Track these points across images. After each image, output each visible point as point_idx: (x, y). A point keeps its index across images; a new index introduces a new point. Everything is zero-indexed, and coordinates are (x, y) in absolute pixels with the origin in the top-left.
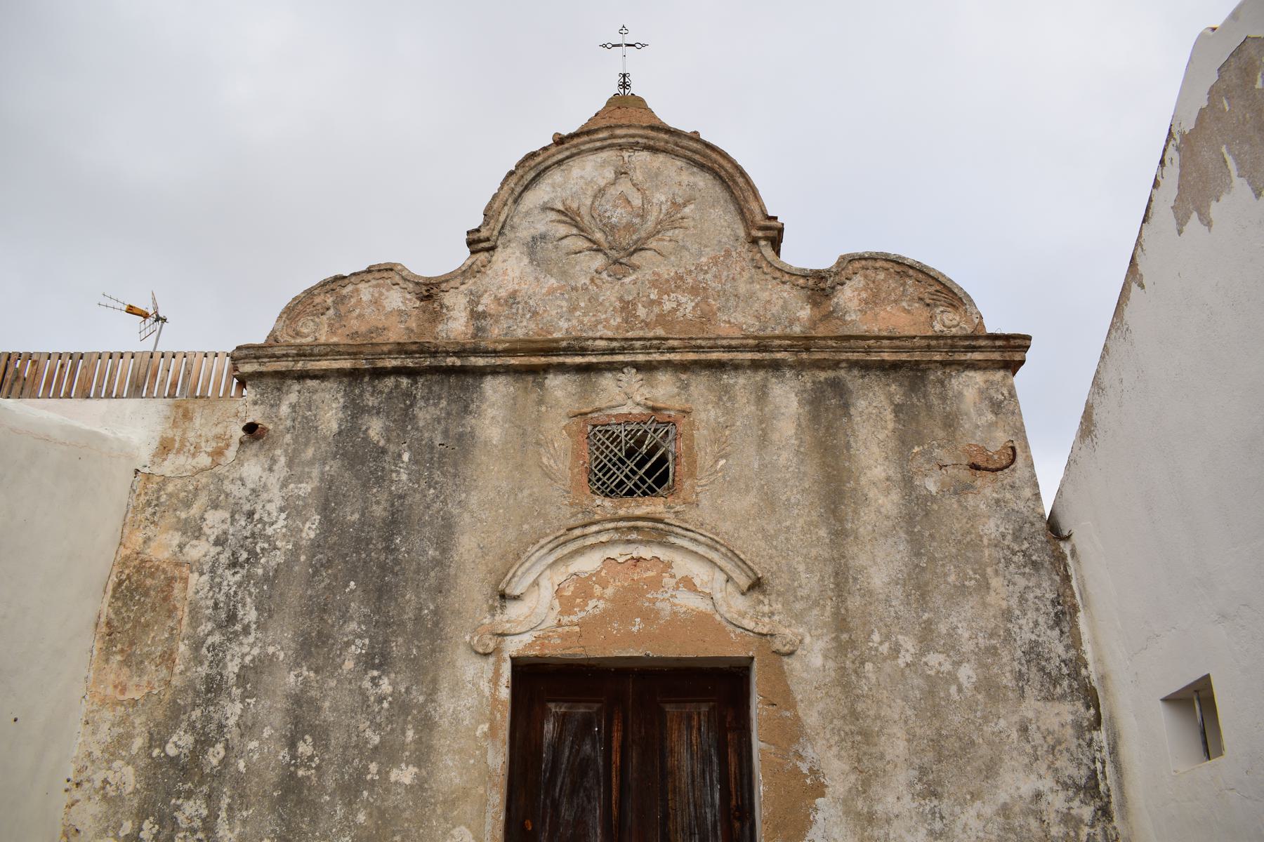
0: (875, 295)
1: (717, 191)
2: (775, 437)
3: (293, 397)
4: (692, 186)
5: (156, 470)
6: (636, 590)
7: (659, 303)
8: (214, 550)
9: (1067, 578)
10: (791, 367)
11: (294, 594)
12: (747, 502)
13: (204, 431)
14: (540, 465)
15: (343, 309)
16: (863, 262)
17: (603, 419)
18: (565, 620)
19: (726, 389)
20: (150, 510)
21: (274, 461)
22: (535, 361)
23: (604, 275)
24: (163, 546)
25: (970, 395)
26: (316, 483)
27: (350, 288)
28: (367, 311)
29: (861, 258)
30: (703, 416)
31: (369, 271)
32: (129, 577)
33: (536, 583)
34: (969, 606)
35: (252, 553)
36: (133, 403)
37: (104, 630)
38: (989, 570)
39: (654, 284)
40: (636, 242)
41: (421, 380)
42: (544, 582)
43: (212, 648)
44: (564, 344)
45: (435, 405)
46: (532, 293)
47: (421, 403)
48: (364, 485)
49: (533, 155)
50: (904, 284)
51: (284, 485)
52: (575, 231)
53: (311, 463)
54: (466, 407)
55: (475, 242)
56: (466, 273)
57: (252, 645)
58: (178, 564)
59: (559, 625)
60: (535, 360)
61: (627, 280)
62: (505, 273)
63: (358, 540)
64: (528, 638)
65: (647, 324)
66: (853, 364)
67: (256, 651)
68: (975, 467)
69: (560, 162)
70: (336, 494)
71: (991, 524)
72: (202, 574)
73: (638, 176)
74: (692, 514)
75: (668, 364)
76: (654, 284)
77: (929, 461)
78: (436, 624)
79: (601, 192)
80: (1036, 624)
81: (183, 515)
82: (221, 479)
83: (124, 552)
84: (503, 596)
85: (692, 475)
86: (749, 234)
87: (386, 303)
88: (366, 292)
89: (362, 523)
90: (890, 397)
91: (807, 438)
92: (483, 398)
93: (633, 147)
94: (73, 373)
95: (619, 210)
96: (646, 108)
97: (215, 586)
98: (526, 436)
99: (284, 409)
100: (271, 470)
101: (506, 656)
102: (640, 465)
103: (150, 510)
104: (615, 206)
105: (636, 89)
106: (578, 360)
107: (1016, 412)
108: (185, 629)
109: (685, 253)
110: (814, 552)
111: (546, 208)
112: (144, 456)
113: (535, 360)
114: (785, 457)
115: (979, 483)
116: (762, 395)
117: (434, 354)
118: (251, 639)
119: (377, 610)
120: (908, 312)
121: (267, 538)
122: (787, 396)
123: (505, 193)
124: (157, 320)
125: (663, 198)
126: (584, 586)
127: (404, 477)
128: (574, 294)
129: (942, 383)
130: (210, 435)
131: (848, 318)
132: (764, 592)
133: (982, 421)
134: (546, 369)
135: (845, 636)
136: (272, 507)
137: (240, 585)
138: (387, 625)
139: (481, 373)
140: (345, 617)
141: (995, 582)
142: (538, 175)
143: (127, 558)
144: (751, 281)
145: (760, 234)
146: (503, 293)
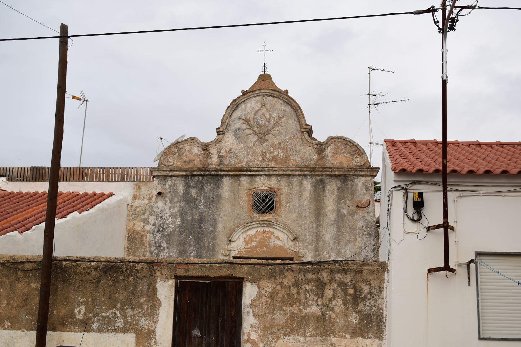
0: (337, 151)
1: (292, 113)
2: (303, 197)
3: (169, 182)
5: (133, 204)
6: (264, 239)
7: (273, 153)
8: (153, 227)
9: (378, 239)
10: (310, 175)
11: (176, 240)
12: (295, 216)
13: (145, 192)
14: (239, 204)
15: (181, 153)
16: (335, 139)
17: (256, 191)
18: (246, 247)
19: (291, 182)
20: (134, 216)
21: (166, 202)
22: (237, 173)
23: (257, 143)
24: (139, 226)
25: (360, 184)
26: (178, 208)
27: (182, 146)
28: (188, 154)
29: (334, 138)
30: (284, 190)
31: (187, 140)
32: (131, 235)
33: (239, 237)
34: (350, 245)
35: (163, 228)
36: (123, 184)
37: (127, 249)
38: (357, 236)
39: (272, 146)
40: (267, 131)
41: (205, 178)
42: (241, 237)
43: (156, 253)
44: (245, 169)
45: (210, 185)
46: (238, 150)
47: (206, 185)
48: (192, 209)
50: (346, 147)
51: (170, 209)
52: (248, 127)
53: (177, 202)
54: (218, 186)
55: (219, 132)
57: (166, 253)
58: (144, 231)
59: (245, 248)
60: (237, 173)
61: (264, 145)
62: (228, 142)
63: (192, 225)
64: (237, 252)
65: (270, 160)
66: (327, 175)
67: (167, 255)
68: (358, 207)
69: (244, 101)
70: (184, 212)
71: (360, 223)
72: (150, 234)
73: (268, 106)
74: (280, 219)
75: (275, 174)
76: (272, 146)
77: (345, 205)
78: (213, 248)
79: (256, 112)
80: (368, 251)
81: (143, 217)
82: (152, 207)
83: (128, 228)
84: (230, 241)
85: (280, 208)
86: (301, 130)
87: (193, 151)
88: (187, 147)
90: (337, 185)
91: (312, 197)
92: (223, 184)
93: (267, 96)
94: (103, 173)
95: (262, 119)
96: (272, 81)
97: (154, 237)
98: (235, 196)
99: (167, 186)
100: (165, 204)
101: (231, 256)
102: (266, 204)
103: (134, 216)
104: (261, 118)
105: (269, 71)
106: (250, 173)
108: (148, 248)
109: (282, 135)
110: (311, 230)
111: (240, 118)
112: (130, 200)
113: (237, 173)
114: (306, 203)
115: (358, 211)
116: (301, 184)
117: (209, 171)
118: (166, 251)
119: (198, 244)
120: (346, 157)
121: (167, 224)
122: (308, 185)
123: (227, 115)
124: (84, 101)
125: (276, 115)
126: (251, 238)
127: (203, 207)
128: (248, 149)
129: (352, 180)
130: (147, 194)
131: (328, 159)
132: (297, 241)
134: (241, 175)
135: (317, 253)
136: (167, 215)
137: (161, 237)
138: (201, 248)
139: (222, 176)
140: (190, 246)
141: (359, 239)
142: (237, 106)
143: (129, 230)
144: (301, 146)
145: (304, 130)
146: (227, 149)
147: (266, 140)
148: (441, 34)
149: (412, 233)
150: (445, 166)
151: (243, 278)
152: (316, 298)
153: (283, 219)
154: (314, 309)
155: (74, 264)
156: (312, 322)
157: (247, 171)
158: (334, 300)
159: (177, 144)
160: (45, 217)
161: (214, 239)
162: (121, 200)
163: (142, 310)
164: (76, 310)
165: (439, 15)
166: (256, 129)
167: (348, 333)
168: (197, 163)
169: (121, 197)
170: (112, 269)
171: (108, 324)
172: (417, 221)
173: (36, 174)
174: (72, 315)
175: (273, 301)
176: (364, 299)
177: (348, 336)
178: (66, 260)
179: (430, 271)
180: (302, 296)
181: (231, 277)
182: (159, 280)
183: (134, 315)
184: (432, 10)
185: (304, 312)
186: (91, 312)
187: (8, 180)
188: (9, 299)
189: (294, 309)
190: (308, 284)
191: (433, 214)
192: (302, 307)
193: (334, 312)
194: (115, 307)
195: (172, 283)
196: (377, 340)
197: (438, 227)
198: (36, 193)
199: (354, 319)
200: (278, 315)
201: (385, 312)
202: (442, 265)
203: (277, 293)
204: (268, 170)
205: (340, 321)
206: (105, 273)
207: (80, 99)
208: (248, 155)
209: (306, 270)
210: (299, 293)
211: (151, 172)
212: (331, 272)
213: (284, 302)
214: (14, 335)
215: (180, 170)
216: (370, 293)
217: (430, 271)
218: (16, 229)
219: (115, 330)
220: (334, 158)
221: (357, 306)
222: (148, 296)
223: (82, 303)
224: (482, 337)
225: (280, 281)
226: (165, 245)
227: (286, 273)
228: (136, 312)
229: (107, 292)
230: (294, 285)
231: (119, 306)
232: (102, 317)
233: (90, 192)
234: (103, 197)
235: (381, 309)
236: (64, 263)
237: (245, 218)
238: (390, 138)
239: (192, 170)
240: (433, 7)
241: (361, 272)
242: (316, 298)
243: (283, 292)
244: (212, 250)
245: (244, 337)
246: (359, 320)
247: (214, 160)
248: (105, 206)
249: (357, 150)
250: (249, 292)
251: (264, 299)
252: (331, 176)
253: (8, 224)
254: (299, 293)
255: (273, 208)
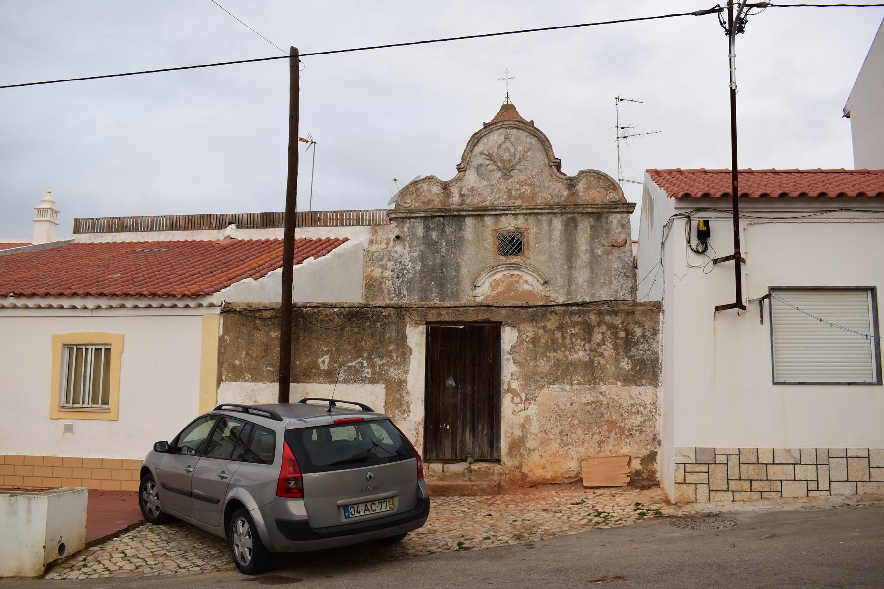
1: (540, 146)
3: (408, 225)
4: (531, 143)
6: (512, 284)
9: (636, 280)
11: (417, 286)
19: (539, 221)
22: (481, 213)
24: (377, 273)
25: (615, 222)
29: (586, 172)
31: (425, 178)
34: (606, 288)
46: (481, 188)
49: (476, 133)
53: (416, 246)
55: (459, 169)
56: (457, 180)
60: (481, 213)
64: (482, 298)
66: (578, 213)
68: (613, 246)
73: (513, 139)
74: (528, 261)
79: (500, 146)
88: (425, 187)
89: (434, 265)
92: (465, 225)
93: (511, 127)
98: (479, 238)
99: (406, 229)
105: (512, 101)
106: (494, 213)
107: (629, 228)
108: (387, 296)
111: (482, 153)
112: (366, 245)
113: (481, 213)
114: (556, 243)
116: (550, 223)
126: (497, 283)
133: (617, 231)
134: (484, 215)
136: (407, 260)
139: (465, 216)
140: (432, 292)
141: (614, 282)
146: (469, 187)
147: (512, 177)
148: (728, 37)
149: (697, 267)
150: (735, 189)
151: (501, 323)
152: (583, 343)
153: (532, 261)
154: (581, 355)
155: (316, 310)
156: (579, 369)
157: (491, 210)
158: (603, 344)
159: (415, 183)
160: (282, 262)
161: (457, 284)
162: (357, 245)
163: (392, 359)
164: (320, 360)
165: (725, 15)
166: (499, 164)
167: (619, 380)
168: (437, 203)
169: (357, 242)
170: (356, 316)
171: (355, 375)
172: (703, 253)
173: (267, 220)
174: (316, 366)
175: (535, 346)
176: (636, 343)
177: (619, 383)
178: (306, 307)
179: (717, 309)
180: (568, 341)
181: (488, 321)
182: (408, 326)
183: (383, 364)
184: (718, 10)
185: (570, 358)
186: (336, 362)
187: (238, 227)
188: (248, 349)
189: (559, 355)
190: (574, 327)
191: (721, 243)
192: (567, 353)
193: (603, 357)
194: (362, 356)
195: (422, 328)
196: (652, 388)
197: (727, 258)
198: (267, 241)
199: (626, 364)
200: (541, 362)
201: (660, 357)
202: (734, 301)
203: (540, 338)
204: (515, 209)
205: (611, 368)
206: (349, 319)
207: (307, 141)
208: (492, 192)
209: (571, 311)
210: (563, 338)
211: (388, 214)
212: (600, 313)
213: (547, 348)
214: (256, 388)
215: (419, 211)
216: (644, 336)
217: (717, 309)
218: (250, 276)
219: (363, 381)
220: (586, 194)
221: (630, 350)
222: (397, 344)
223: (326, 353)
224: (875, 381)
225: (543, 324)
226: (406, 292)
227: (549, 316)
228: (384, 361)
229: (352, 340)
230: (558, 328)
231: (366, 355)
232: (348, 366)
233: (323, 238)
234: (337, 242)
235: (656, 353)
236: (305, 310)
237: (490, 261)
238: (652, 167)
239: (432, 210)
240: (719, 6)
241: (633, 313)
242: (583, 343)
243: (546, 337)
244: (456, 296)
245: (505, 387)
246: (632, 365)
247: (456, 199)
248: (342, 251)
249: (612, 185)
250: (509, 337)
251: (525, 345)
252: (583, 213)
253: (242, 271)
254: (563, 338)
255: (520, 250)
